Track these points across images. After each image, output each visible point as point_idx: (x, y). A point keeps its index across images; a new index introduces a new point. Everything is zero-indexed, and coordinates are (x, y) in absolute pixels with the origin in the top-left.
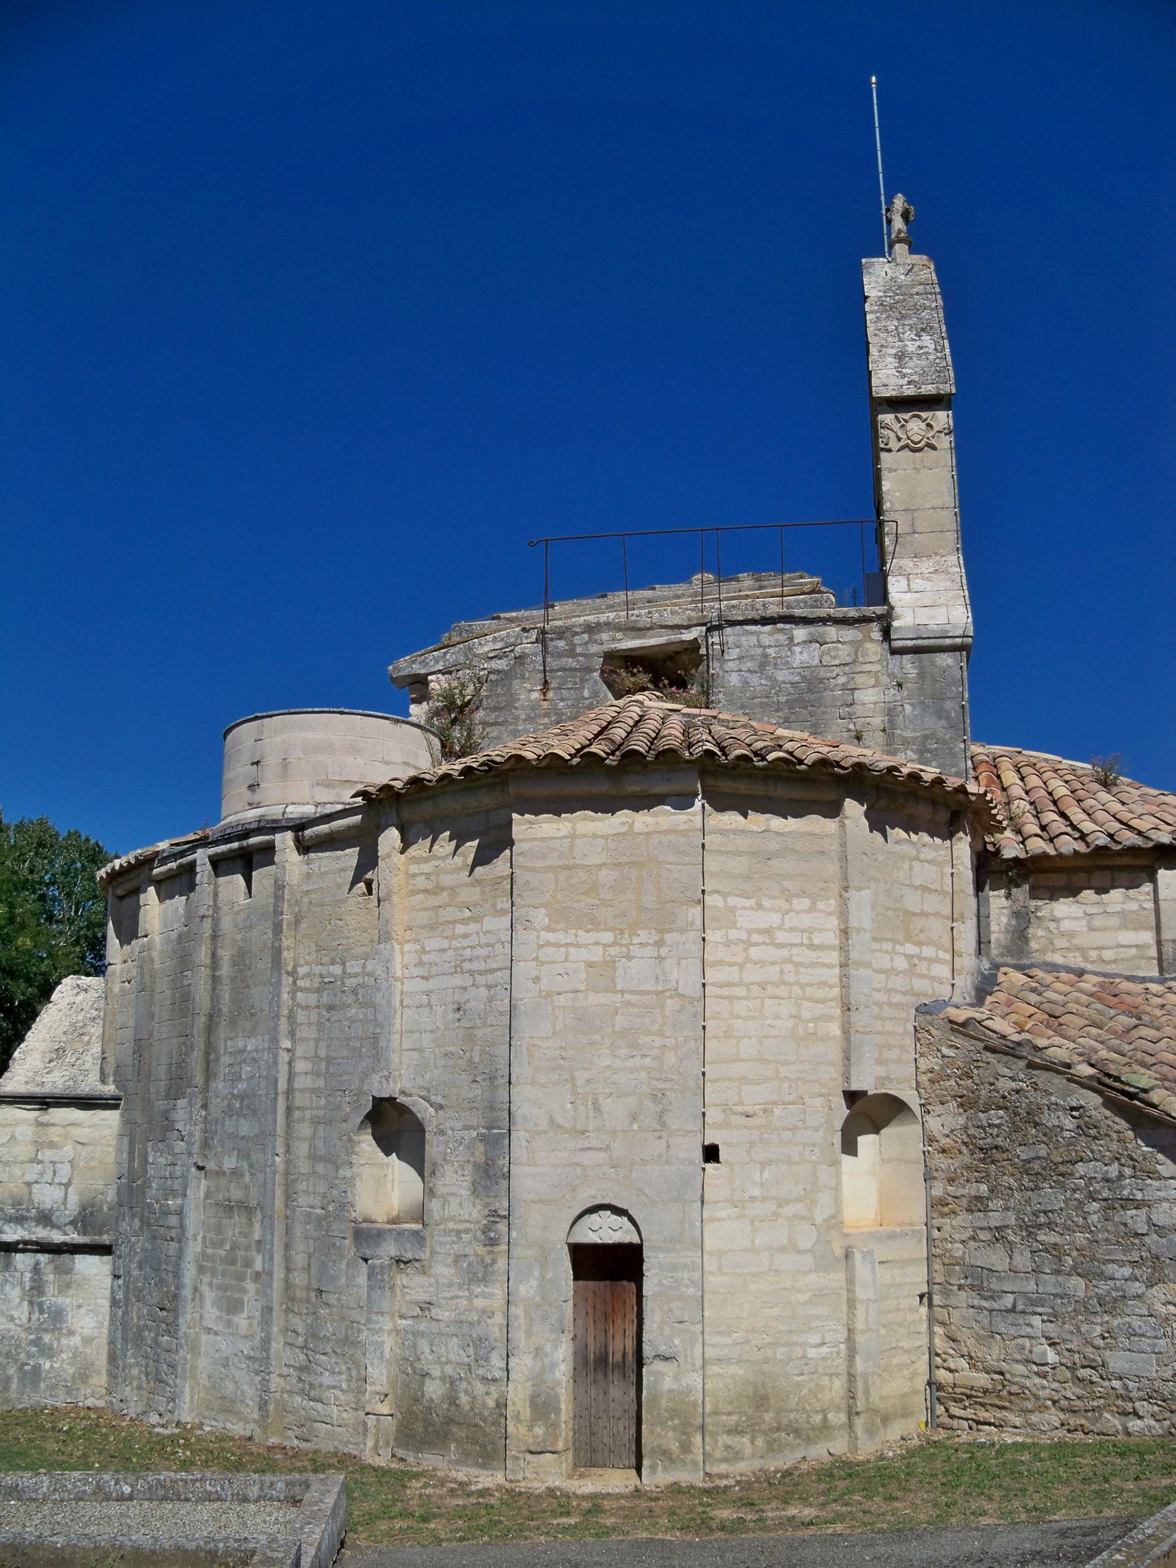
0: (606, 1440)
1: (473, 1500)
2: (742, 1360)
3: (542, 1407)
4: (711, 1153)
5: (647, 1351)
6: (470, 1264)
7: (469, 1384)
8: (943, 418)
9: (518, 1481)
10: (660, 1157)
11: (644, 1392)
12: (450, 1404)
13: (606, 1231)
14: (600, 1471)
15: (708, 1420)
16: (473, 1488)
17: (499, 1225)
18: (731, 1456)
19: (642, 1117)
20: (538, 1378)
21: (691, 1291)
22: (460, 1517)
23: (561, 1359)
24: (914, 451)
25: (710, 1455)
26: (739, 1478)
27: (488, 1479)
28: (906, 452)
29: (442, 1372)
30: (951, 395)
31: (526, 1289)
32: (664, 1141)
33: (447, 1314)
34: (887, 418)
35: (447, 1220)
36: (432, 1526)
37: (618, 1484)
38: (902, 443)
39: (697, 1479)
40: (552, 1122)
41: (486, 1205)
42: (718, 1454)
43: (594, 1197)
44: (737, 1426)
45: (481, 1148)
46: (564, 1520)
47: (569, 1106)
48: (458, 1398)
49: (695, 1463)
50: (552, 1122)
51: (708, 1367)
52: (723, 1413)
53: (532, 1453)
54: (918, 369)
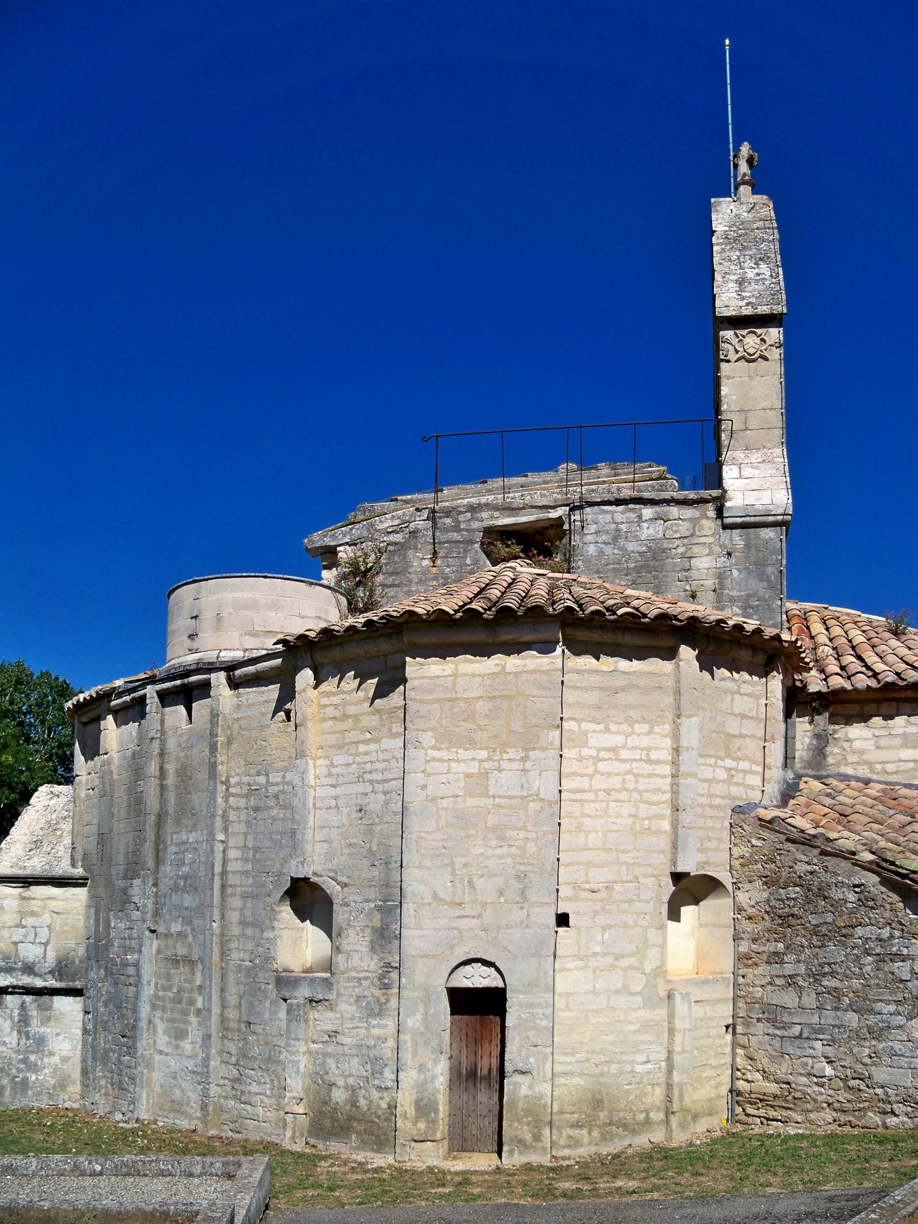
0: (474, 1132)
1: (369, 1175)
2: (584, 1074)
3: (424, 1108)
5: (508, 1067)
6: (368, 1003)
7: (367, 1091)
8: (774, 334)
10: (522, 922)
12: (352, 1106)
15: (555, 1118)
17: (392, 974)
18: (572, 1144)
20: (422, 1087)
22: (359, 1188)
23: (440, 1073)
24: (749, 361)
25: (556, 1143)
27: (380, 1160)
28: (743, 363)
29: (346, 1082)
30: (783, 314)
31: (413, 1022)
32: (525, 911)
33: (350, 1040)
34: (728, 334)
36: (337, 1194)
38: (739, 355)
39: (546, 1161)
40: (435, 896)
42: (562, 1142)
43: (468, 953)
45: (378, 916)
46: (441, 1190)
47: (449, 884)
49: (544, 1149)
50: (435, 896)
53: (416, 1141)
54: (755, 293)
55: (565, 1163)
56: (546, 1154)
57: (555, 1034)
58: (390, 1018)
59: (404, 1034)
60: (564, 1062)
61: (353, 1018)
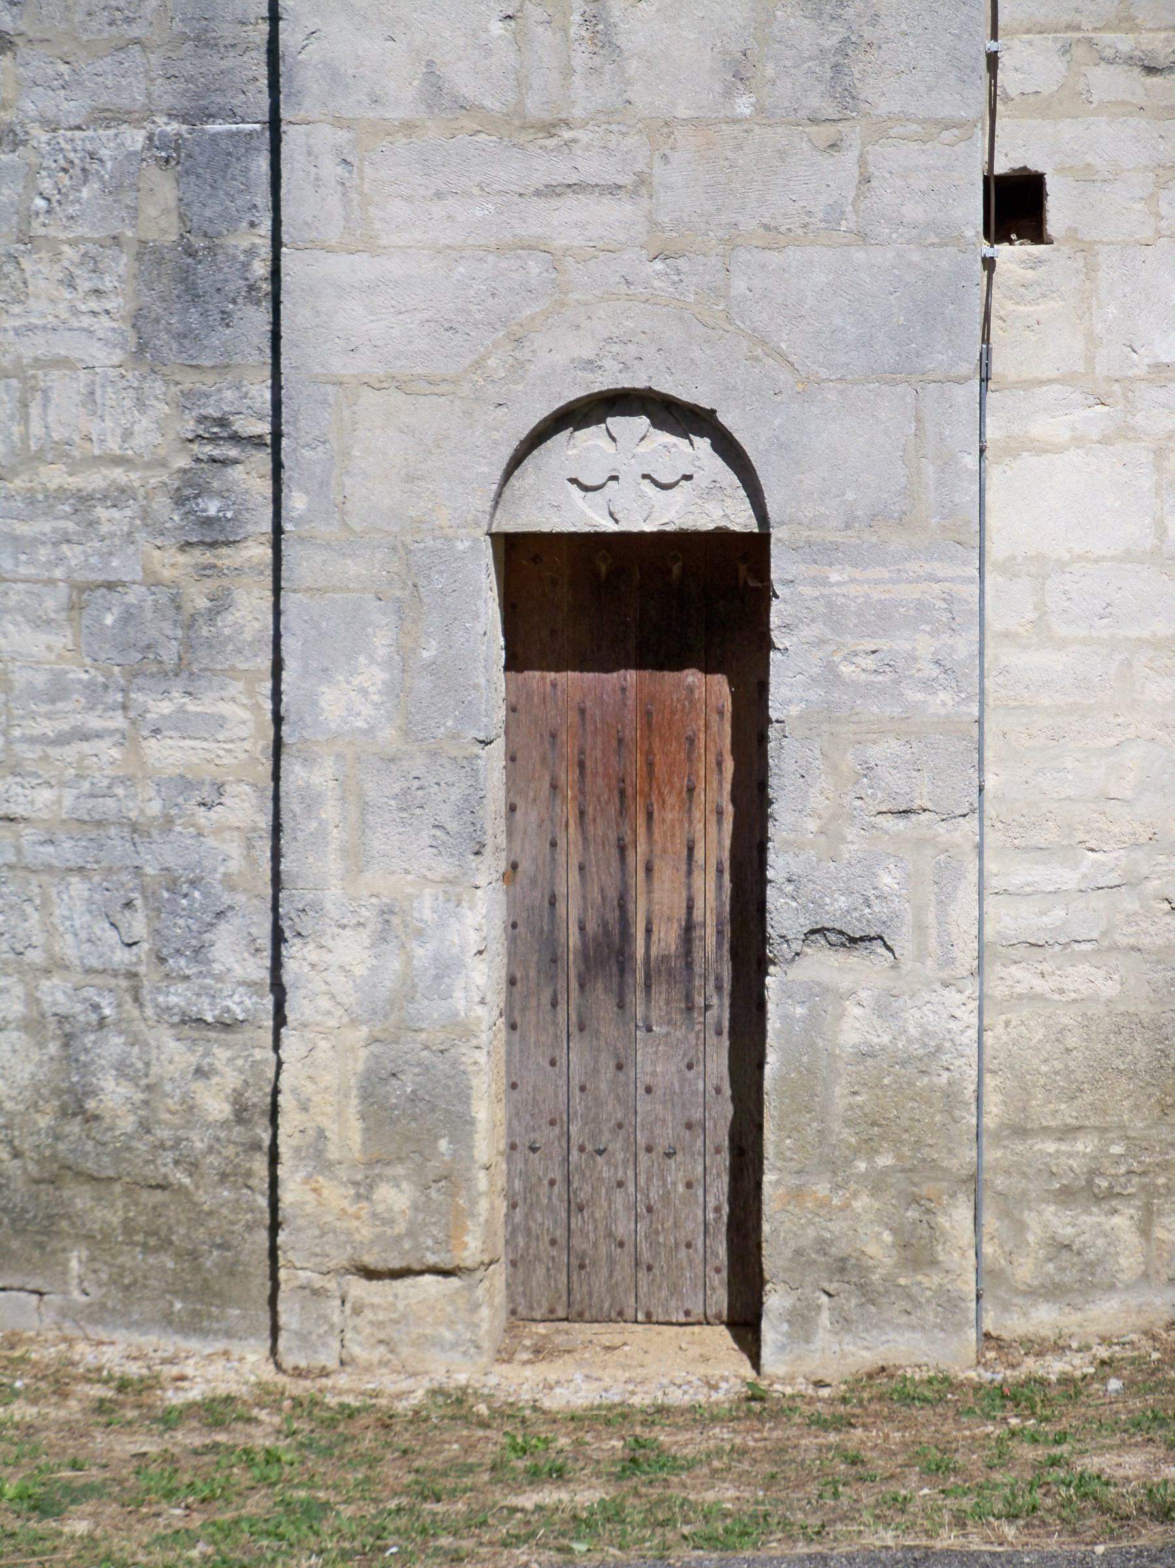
0: (622, 1229)
1: (189, 1437)
2: (1114, 948)
3: (405, 1114)
4: (1016, 205)
5: (784, 914)
6: (128, 617)
7: (135, 1040)
9: (324, 1373)
10: (834, 215)
12: (64, 1113)
14: (606, 1333)
15: (992, 1155)
16: (174, 1398)
17: (236, 473)
18: (1068, 1277)
19: (770, 71)
20: (390, 1018)
21: (942, 702)
22: (169, 1494)
23: (469, 938)
25: (997, 1275)
26: (1103, 1353)
27: (219, 1366)
29: (32, 1000)
31: (344, 699)
32: (850, 158)
33: (45, 795)
35: (39, 457)
36: (81, 1527)
37: (680, 1375)
39: (955, 1355)
40: (435, 90)
42: (1025, 1271)
43: (590, 365)
44: (1093, 1173)
45: (163, 190)
46: (549, 1496)
47: (497, 28)
48: (93, 1093)
49: (949, 1303)
50: (435, 90)
51: (995, 970)
53: (370, 1274)
55: (1054, 1367)
56: (959, 1327)
57: (989, 754)
58: (236, 688)
59: (308, 761)
60: (1034, 891)
61: (57, 691)
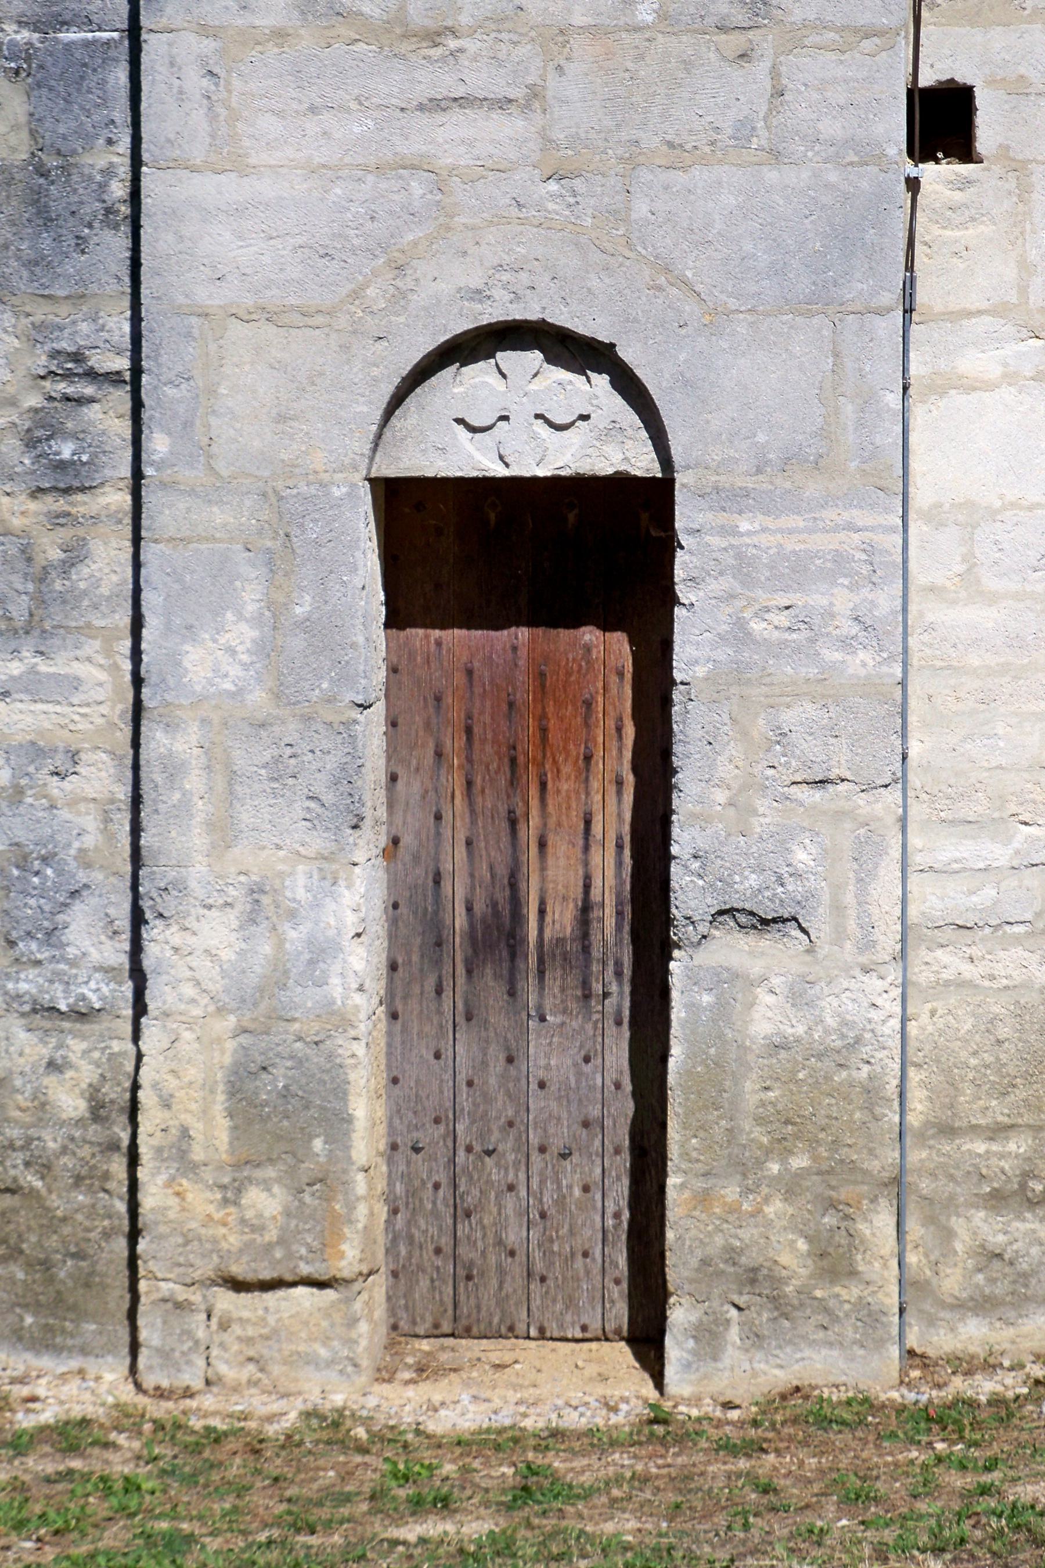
0: (513, 1236)
3: (277, 1111)
4: (942, 122)
5: (689, 893)
10: (744, 131)
11: (677, 1051)
13: (531, 428)
14: (495, 1350)
17: (92, 412)
20: (262, 1005)
21: (862, 662)
25: (922, 1287)
31: (211, 659)
32: (761, 68)
39: (873, 1373)
41: (40, 332)
42: (952, 1282)
43: (478, 295)
44: (1027, 1175)
49: (869, 1316)
51: (919, 955)
52: (974, 1129)
53: (238, 1286)
